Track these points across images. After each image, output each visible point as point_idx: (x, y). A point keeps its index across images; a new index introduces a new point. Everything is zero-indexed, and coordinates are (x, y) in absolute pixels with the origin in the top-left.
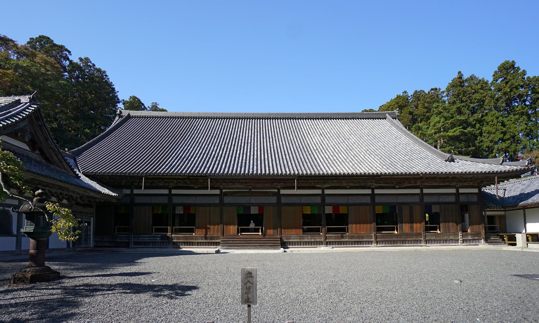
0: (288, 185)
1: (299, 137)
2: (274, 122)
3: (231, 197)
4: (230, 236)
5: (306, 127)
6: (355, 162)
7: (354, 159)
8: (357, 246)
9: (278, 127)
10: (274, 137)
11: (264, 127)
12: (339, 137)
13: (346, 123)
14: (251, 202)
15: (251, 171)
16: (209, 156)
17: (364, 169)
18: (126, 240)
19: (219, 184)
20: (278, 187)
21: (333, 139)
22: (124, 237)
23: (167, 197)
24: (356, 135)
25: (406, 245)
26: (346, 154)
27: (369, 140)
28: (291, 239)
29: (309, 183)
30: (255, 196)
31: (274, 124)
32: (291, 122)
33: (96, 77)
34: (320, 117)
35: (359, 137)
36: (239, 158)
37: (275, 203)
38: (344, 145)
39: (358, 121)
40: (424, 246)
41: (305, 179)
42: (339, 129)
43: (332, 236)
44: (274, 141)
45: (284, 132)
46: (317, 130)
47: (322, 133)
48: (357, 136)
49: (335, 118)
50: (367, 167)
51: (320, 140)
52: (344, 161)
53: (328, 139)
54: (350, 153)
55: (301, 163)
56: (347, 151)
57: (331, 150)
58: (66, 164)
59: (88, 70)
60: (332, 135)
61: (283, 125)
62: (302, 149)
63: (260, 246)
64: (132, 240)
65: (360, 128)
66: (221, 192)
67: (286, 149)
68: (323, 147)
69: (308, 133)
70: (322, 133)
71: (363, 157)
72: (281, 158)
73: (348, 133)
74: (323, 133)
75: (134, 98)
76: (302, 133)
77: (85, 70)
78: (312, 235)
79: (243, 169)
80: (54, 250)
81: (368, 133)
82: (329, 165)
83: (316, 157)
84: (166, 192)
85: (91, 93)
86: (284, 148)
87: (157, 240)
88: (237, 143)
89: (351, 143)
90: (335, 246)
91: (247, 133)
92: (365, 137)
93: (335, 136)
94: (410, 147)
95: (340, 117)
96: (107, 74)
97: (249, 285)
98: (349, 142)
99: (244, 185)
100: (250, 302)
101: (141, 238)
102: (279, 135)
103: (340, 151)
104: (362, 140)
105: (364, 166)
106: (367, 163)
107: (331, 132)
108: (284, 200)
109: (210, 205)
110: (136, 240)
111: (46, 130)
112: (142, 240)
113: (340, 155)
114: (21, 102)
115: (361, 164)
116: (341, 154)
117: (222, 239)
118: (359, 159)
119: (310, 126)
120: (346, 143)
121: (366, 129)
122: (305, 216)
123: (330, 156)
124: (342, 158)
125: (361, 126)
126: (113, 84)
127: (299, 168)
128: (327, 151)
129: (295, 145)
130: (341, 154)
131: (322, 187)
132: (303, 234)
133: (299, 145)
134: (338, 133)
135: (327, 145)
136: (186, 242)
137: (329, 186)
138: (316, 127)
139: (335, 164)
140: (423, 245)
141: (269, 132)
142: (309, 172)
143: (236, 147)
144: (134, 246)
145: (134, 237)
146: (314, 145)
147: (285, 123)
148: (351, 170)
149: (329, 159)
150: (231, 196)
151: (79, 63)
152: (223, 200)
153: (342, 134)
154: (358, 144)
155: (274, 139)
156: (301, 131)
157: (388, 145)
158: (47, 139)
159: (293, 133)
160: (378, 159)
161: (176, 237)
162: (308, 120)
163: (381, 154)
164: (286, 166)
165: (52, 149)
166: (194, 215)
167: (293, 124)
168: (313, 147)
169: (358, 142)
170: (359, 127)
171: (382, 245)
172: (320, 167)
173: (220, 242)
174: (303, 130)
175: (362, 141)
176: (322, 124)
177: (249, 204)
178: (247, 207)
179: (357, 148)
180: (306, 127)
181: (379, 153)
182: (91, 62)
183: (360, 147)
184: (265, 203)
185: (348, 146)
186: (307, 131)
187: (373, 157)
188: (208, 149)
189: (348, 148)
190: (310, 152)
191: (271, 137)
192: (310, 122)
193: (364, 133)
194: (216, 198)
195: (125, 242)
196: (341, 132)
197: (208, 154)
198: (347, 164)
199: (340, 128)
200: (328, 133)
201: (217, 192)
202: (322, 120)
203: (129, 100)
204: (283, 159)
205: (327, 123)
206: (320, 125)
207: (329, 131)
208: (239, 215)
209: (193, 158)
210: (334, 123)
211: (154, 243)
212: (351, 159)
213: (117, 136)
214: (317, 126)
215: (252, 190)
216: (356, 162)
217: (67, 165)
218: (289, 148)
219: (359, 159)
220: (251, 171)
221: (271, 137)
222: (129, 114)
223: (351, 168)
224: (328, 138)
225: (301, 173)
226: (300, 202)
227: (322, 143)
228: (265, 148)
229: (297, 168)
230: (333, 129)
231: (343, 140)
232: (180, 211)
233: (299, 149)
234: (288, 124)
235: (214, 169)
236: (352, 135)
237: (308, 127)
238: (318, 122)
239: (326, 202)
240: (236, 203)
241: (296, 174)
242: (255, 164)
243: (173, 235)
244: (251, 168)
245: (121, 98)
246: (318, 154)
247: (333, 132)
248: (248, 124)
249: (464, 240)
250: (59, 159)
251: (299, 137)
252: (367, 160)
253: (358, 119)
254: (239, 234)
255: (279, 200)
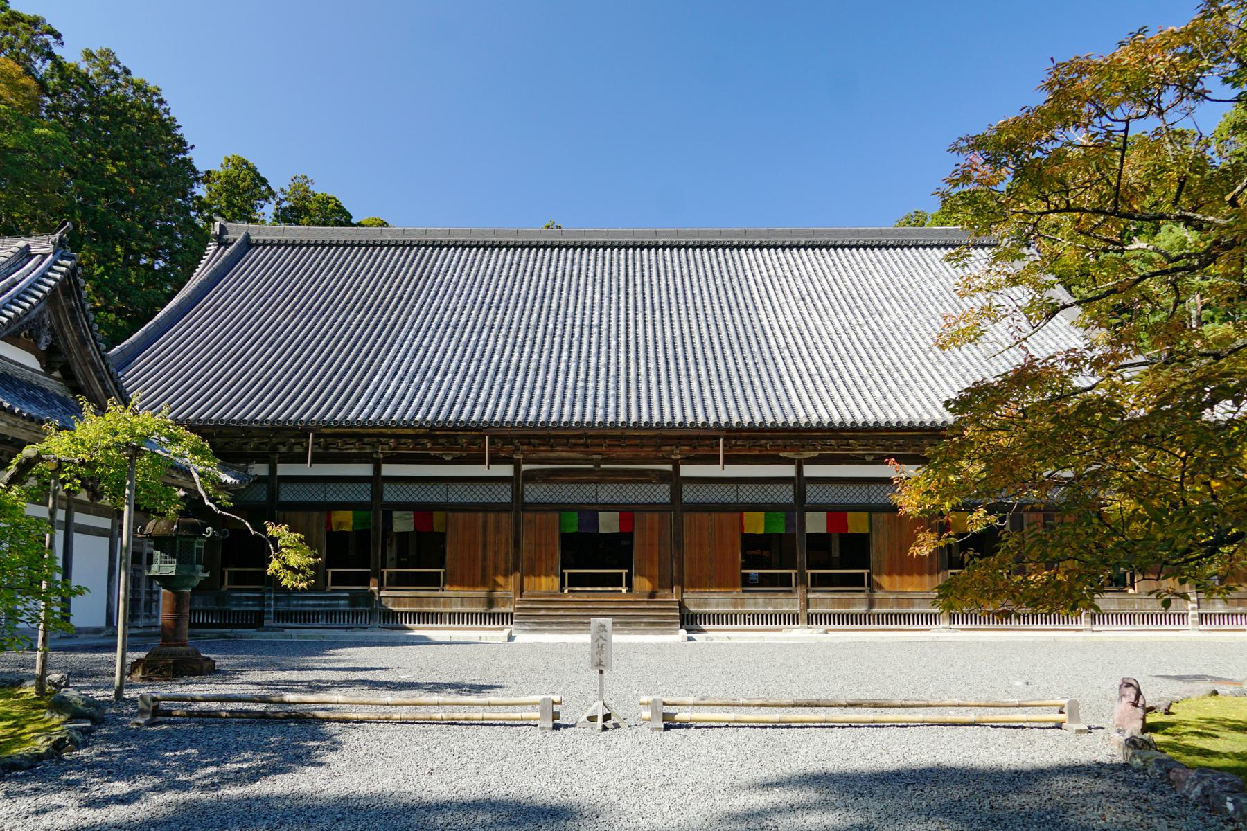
0: (703, 450)
1: (738, 305)
2: (668, 258)
3: (544, 486)
4: (541, 596)
6: (889, 388)
7: (888, 378)
8: (894, 626)
9: (678, 274)
10: (665, 306)
11: (638, 274)
12: (853, 305)
13: (879, 261)
14: (600, 500)
15: (600, 412)
16: (482, 368)
17: (910, 410)
18: (254, 605)
19: (512, 448)
20: (673, 457)
21: (836, 313)
22: (248, 599)
23: (369, 486)
24: (904, 300)
26: (868, 362)
28: (709, 605)
29: (761, 446)
30: (612, 482)
31: (669, 264)
32: (717, 257)
33: (132, 106)
34: (803, 243)
35: (914, 307)
36: (567, 373)
37: (667, 504)
38: (864, 332)
39: (917, 254)
40: (1086, 630)
41: (748, 438)
42: (856, 281)
43: (824, 601)
44: (667, 319)
45: (696, 290)
46: (793, 285)
47: (804, 292)
48: (907, 304)
49: (847, 243)
50: (920, 401)
51: (798, 317)
52: (860, 382)
53: (823, 313)
54: (879, 357)
55: (738, 391)
56: (872, 352)
57: (826, 347)
59: (108, 88)
60: (833, 300)
61: (692, 266)
62: (745, 347)
64: (269, 605)
65: (918, 278)
66: (517, 470)
67: (698, 346)
68: (804, 339)
69: (764, 294)
70: (804, 292)
71: (914, 372)
72: (683, 372)
73: (880, 295)
74: (809, 294)
76: (747, 294)
77: (99, 86)
78: (769, 595)
79: (578, 408)
80: (79, 631)
81: (941, 294)
82: (815, 396)
83: (783, 370)
84: (365, 470)
85: (116, 157)
86: (693, 343)
87: (338, 605)
88: (559, 326)
89: (887, 327)
90: (832, 626)
91: (589, 294)
92: (930, 307)
93: (843, 302)
94: (1056, 338)
95: (861, 242)
96: (164, 96)
97: (601, 642)
98: (881, 323)
99: (582, 452)
101: (295, 602)
102: (682, 301)
103: (853, 352)
104: (920, 316)
105: (913, 400)
106: (922, 390)
107: (832, 290)
108: (690, 495)
109: (485, 508)
110: (282, 607)
112: (297, 606)
114: (33, 251)
115: (904, 394)
116: (853, 361)
117: (518, 604)
118: (902, 377)
119: (772, 272)
120: (874, 326)
121: (936, 282)
122: (750, 541)
123: (822, 368)
124: (856, 375)
125: (921, 272)
126: (177, 124)
127: (731, 405)
128: (814, 352)
129: (727, 331)
130: (853, 361)
131: (797, 457)
132: (743, 591)
133: (737, 332)
134: (854, 292)
136: (419, 613)
137: (816, 454)
138: (789, 274)
139: (834, 392)
140: (1083, 626)
141: (652, 291)
142: (758, 419)
143: (557, 340)
144: (276, 624)
145: (277, 599)
146: (778, 334)
147: (699, 261)
148: (873, 413)
149: (817, 378)
150: (545, 481)
151: (83, 67)
152: (523, 493)
153: (865, 297)
154: (907, 328)
155: (666, 313)
156: (745, 287)
158: (83, 342)
159: (722, 293)
160: (954, 378)
161: (389, 597)
162: (769, 250)
163: (966, 363)
164: (697, 399)
165: (93, 364)
166: (442, 537)
167: (723, 265)
168: (776, 338)
169: (907, 322)
170: (915, 274)
171: (965, 626)
172: (789, 400)
174: (752, 282)
175: (919, 321)
176: (808, 264)
177: (593, 504)
178: (589, 513)
179: (903, 342)
181: (964, 360)
182: (117, 64)
183: (910, 340)
184: (637, 504)
185: (876, 338)
186: (762, 288)
187: (943, 371)
188: (480, 348)
189: (875, 342)
190: (767, 356)
191: (657, 306)
192: (774, 257)
193: (928, 292)
194: (503, 487)
195: (252, 612)
196: (862, 292)
198: (866, 393)
199: (861, 277)
200: (822, 295)
201: (506, 470)
202: (810, 250)
203: (221, 170)
204: (688, 375)
205: (822, 262)
206: (802, 267)
207: (827, 288)
209: (440, 373)
210: (844, 260)
211: (329, 615)
212: (878, 379)
213: (219, 306)
214: (791, 271)
215: (602, 466)
216: (893, 386)
218: (707, 343)
219: (902, 377)
220: (600, 412)
221: (657, 306)
222: (247, 237)
223: (875, 407)
225: (736, 420)
226: (735, 499)
227: (803, 325)
228: (641, 342)
229: (726, 403)
230: (840, 282)
231: (863, 317)
232: (402, 523)
233: (736, 347)
234: (707, 264)
235: (500, 408)
236: (892, 300)
237: (765, 274)
238: (797, 256)
239: (808, 500)
240: (556, 503)
241: (723, 423)
242: (612, 392)
243: (383, 594)
244: (600, 404)
245: (201, 166)
246: (789, 362)
247: (837, 292)
248: (592, 263)
249: (1202, 615)
251: (738, 305)
252: (925, 380)
253: (917, 247)
254: (566, 591)
255: (676, 494)
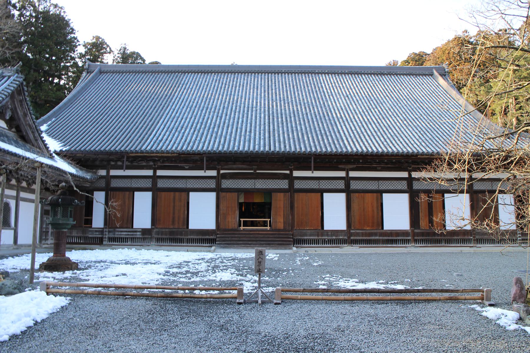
3: (231, 180)
5: (328, 85)
12: (370, 100)
18: (99, 234)
25: (452, 245)
27: (407, 105)
28: (306, 235)
53: (357, 103)
58: (41, 142)
63: (266, 244)
64: (106, 235)
66: (218, 172)
70: (348, 93)
75: (98, 38)
87: (136, 235)
97: (260, 260)
100: (261, 272)
101: (117, 233)
108: (298, 185)
110: (111, 235)
111: (26, 105)
112: (118, 235)
113: (369, 126)
116: (371, 124)
119: (333, 84)
120: (379, 109)
135: (355, 111)
138: (341, 85)
139: (363, 138)
144: (109, 243)
145: (109, 232)
146: (337, 112)
148: (381, 148)
152: (221, 183)
157: (431, 113)
165: (29, 125)
173: (216, 239)
180: (328, 85)
197: (202, 123)
208: (241, 205)
210: (365, 79)
215: (258, 171)
217: (42, 144)
224: (356, 101)
226: (318, 187)
237: (330, 85)
238: (344, 78)
239: (351, 187)
246: (342, 124)
250: (36, 137)
255: (291, 184)
